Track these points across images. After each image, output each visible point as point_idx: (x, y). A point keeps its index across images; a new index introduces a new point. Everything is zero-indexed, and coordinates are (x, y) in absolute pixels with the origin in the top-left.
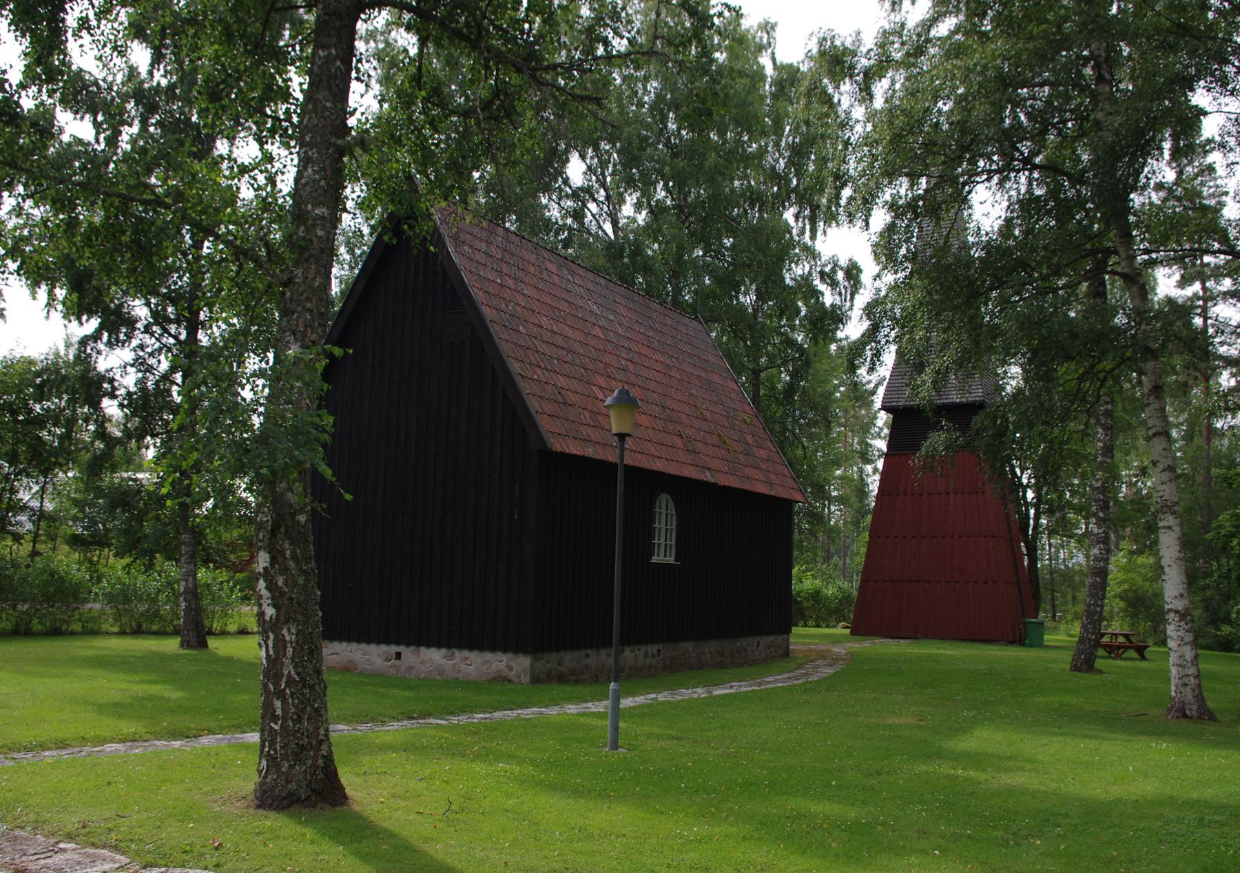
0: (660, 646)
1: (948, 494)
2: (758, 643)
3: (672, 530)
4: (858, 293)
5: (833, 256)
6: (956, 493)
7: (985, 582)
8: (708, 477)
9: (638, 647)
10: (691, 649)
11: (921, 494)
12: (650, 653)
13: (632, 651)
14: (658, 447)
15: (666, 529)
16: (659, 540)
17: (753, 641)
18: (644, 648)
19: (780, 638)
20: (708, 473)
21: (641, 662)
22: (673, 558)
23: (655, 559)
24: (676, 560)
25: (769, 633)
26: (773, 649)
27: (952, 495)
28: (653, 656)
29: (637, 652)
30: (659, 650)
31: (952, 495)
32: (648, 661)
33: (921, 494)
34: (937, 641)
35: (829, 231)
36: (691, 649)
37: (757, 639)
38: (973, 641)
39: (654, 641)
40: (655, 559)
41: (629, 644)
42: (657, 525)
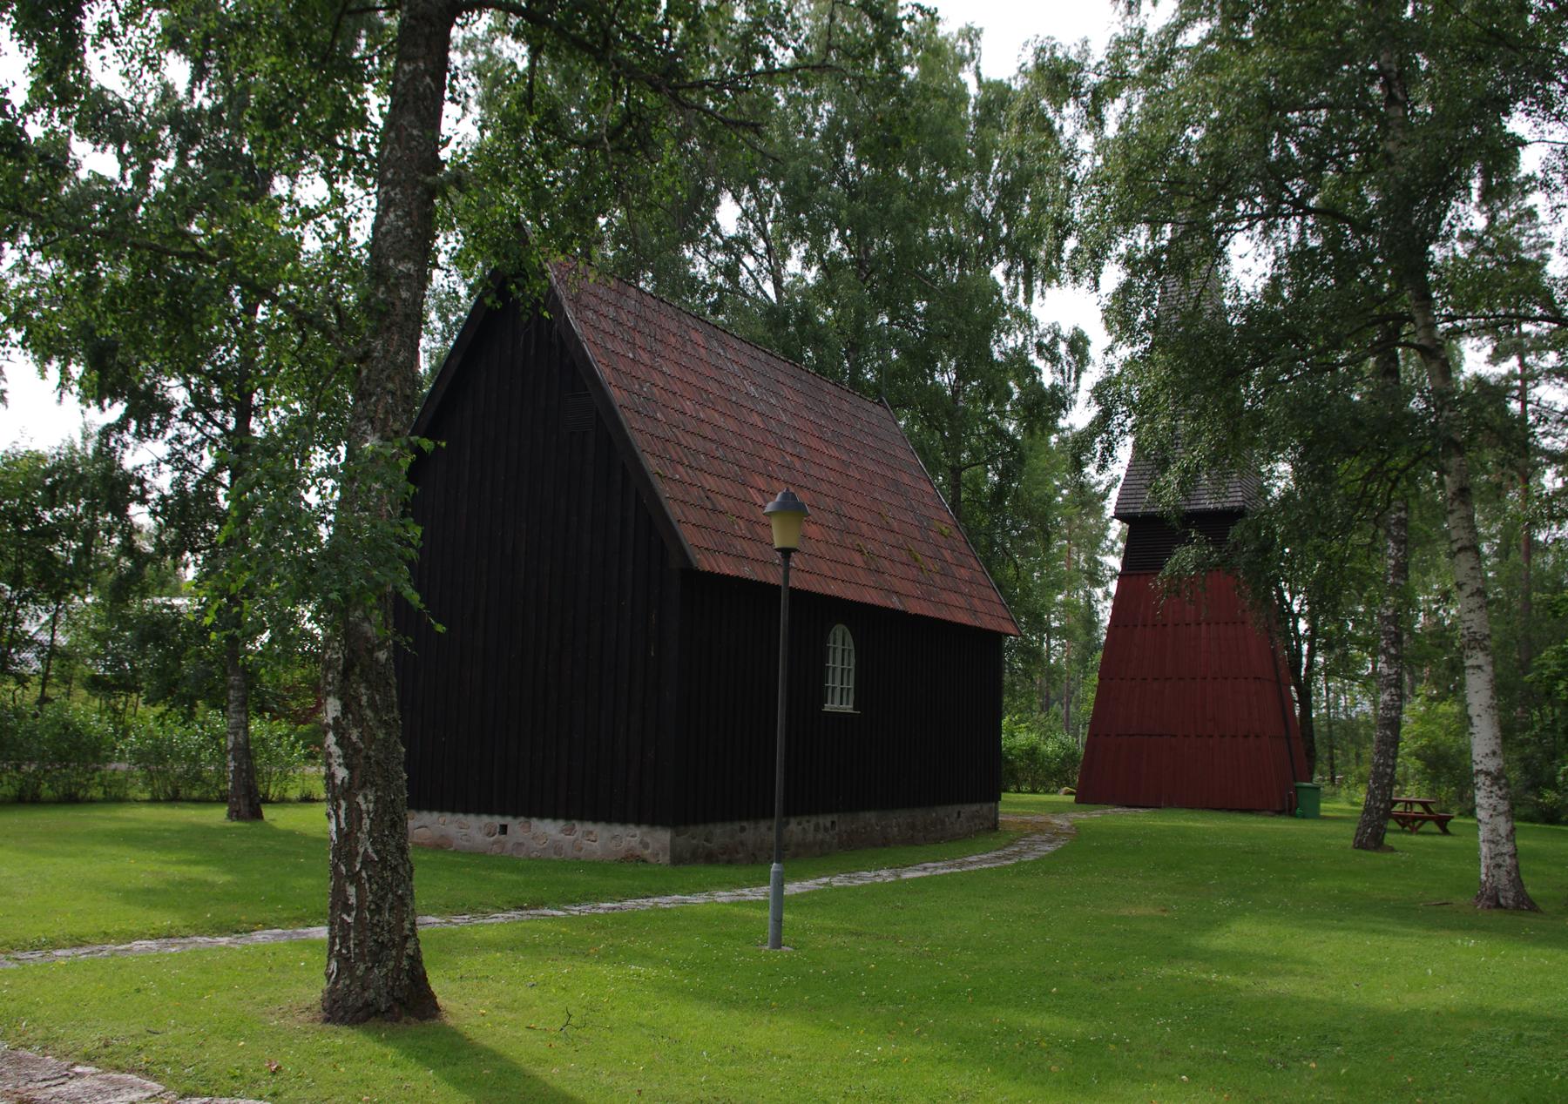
0: (835, 817)
1: (1199, 624)
2: (959, 813)
3: (849, 670)
4: (1085, 370)
5: (1054, 324)
6: (1208, 624)
7: (1246, 737)
8: (895, 603)
9: (807, 818)
10: (873, 821)
11: (1165, 625)
12: (822, 826)
13: (799, 824)
14: (832, 565)
15: (843, 670)
16: (833, 683)
17: (952, 810)
18: (814, 820)
19: (986, 807)
20: (895, 599)
21: (810, 837)
22: (851, 706)
23: (828, 707)
24: (855, 709)
25: (973, 801)
26: (977, 821)
27: (1204, 626)
28: (826, 830)
29: (805, 825)
30: (833, 823)
31: (1204, 626)
32: (820, 836)
33: (1165, 625)
34: (1184, 811)
35: (1048, 292)
36: (873, 821)
37: (957, 808)
38: (1230, 810)
39: (827, 810)
40: (828, 707)
41: (795, 815)
42: (830, 664)
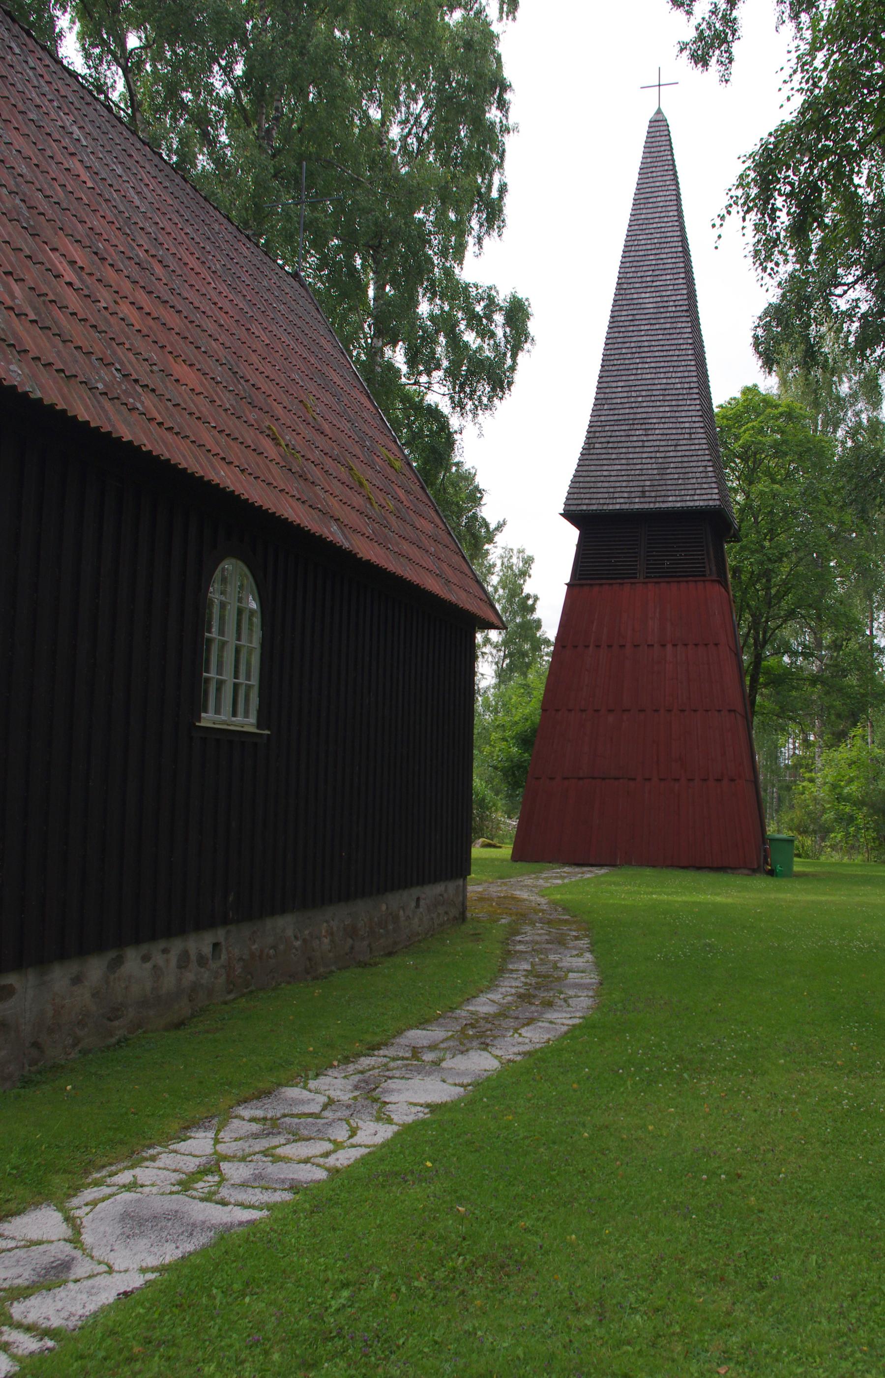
0: (220, 934)
1: (663, 646)
2: (418, 899)
3: (249, 687)
4: (522, 349)
5: (490, 288)
6: (675, 645)
7: (718, 780)
8: (333, 533)
9: (162, 944)
10: (290, 933)
11: (622, 646)
12: (193, 957)
13: (146, 958)
14: (223, 439)
15: (236, 686)
16: (220, 672)
17: (407, 896)
18: (177, 946)
19: (452, 886)
20: (334, 528)
21: (169, 982)
22: (253, 719)
23: (208, 719)
24: (259, 726)
25: (436, 879)
26: (441, 910)
27: (669, 647)
28: (202, 961)
29: (158, 958)
30: (216, 946)
31: (669, 647)
32: (190, 977)
33: (622, 646)
34: (648, 871)
35: (486, 241)
36: (290, 933)
37: (416, 892)
38: (699, 868)
39: (201, 925)
40: (208, 719)
41: (137, 941)
42: (212, 674)
